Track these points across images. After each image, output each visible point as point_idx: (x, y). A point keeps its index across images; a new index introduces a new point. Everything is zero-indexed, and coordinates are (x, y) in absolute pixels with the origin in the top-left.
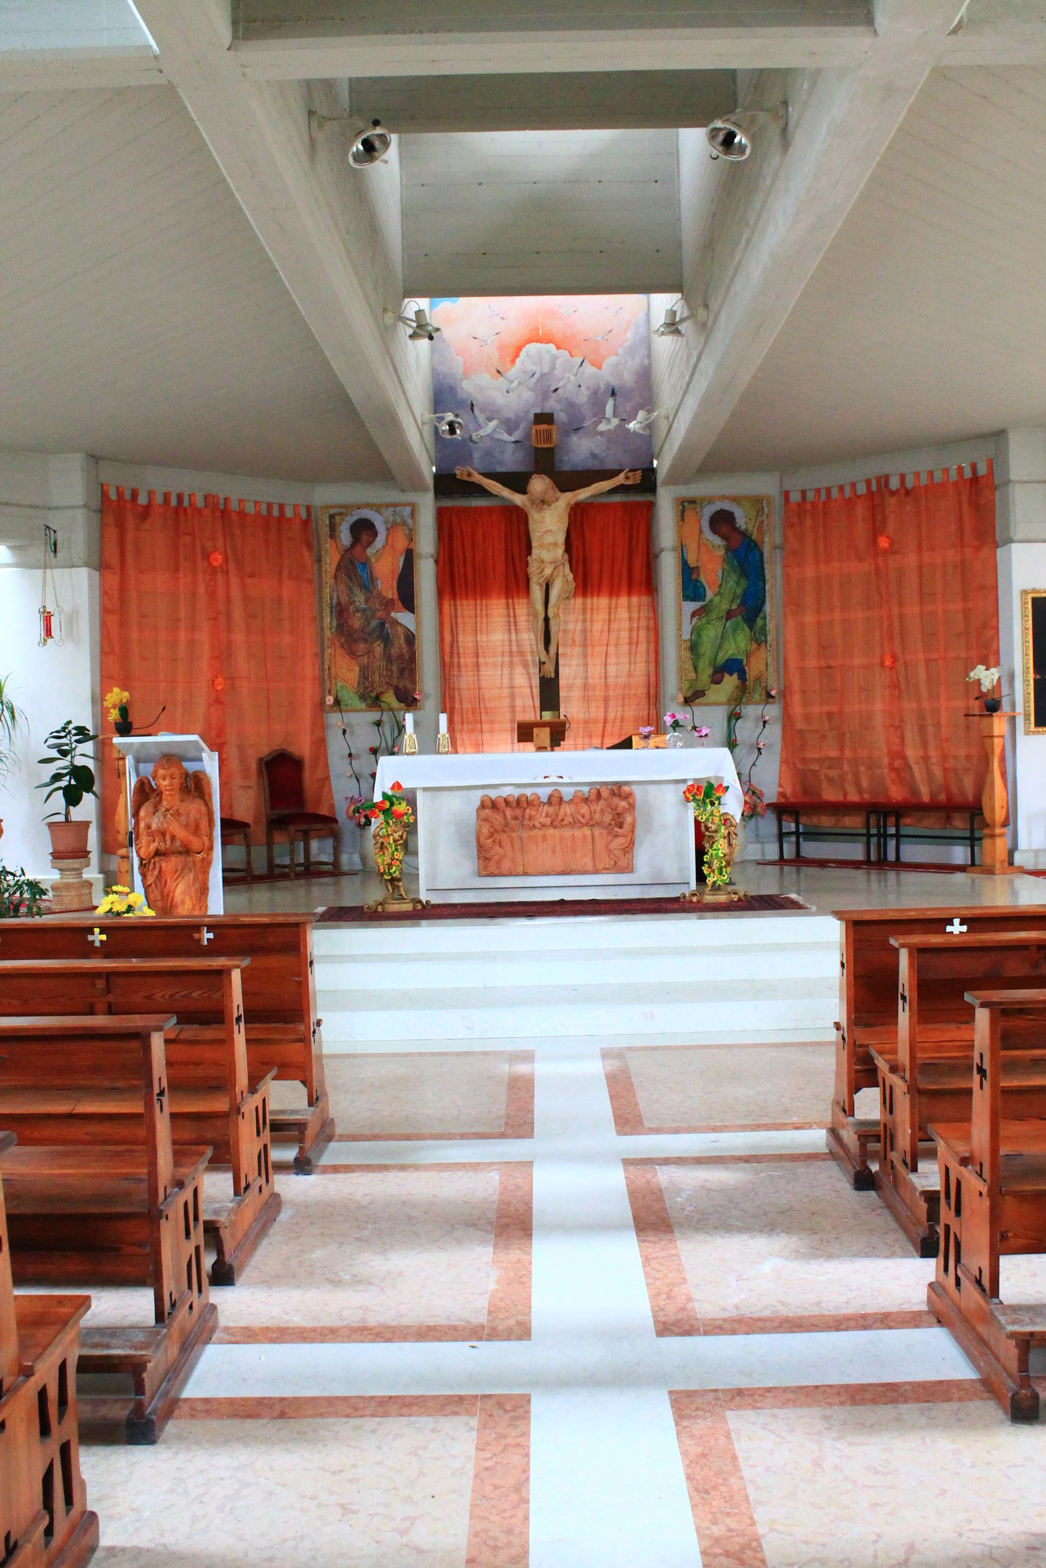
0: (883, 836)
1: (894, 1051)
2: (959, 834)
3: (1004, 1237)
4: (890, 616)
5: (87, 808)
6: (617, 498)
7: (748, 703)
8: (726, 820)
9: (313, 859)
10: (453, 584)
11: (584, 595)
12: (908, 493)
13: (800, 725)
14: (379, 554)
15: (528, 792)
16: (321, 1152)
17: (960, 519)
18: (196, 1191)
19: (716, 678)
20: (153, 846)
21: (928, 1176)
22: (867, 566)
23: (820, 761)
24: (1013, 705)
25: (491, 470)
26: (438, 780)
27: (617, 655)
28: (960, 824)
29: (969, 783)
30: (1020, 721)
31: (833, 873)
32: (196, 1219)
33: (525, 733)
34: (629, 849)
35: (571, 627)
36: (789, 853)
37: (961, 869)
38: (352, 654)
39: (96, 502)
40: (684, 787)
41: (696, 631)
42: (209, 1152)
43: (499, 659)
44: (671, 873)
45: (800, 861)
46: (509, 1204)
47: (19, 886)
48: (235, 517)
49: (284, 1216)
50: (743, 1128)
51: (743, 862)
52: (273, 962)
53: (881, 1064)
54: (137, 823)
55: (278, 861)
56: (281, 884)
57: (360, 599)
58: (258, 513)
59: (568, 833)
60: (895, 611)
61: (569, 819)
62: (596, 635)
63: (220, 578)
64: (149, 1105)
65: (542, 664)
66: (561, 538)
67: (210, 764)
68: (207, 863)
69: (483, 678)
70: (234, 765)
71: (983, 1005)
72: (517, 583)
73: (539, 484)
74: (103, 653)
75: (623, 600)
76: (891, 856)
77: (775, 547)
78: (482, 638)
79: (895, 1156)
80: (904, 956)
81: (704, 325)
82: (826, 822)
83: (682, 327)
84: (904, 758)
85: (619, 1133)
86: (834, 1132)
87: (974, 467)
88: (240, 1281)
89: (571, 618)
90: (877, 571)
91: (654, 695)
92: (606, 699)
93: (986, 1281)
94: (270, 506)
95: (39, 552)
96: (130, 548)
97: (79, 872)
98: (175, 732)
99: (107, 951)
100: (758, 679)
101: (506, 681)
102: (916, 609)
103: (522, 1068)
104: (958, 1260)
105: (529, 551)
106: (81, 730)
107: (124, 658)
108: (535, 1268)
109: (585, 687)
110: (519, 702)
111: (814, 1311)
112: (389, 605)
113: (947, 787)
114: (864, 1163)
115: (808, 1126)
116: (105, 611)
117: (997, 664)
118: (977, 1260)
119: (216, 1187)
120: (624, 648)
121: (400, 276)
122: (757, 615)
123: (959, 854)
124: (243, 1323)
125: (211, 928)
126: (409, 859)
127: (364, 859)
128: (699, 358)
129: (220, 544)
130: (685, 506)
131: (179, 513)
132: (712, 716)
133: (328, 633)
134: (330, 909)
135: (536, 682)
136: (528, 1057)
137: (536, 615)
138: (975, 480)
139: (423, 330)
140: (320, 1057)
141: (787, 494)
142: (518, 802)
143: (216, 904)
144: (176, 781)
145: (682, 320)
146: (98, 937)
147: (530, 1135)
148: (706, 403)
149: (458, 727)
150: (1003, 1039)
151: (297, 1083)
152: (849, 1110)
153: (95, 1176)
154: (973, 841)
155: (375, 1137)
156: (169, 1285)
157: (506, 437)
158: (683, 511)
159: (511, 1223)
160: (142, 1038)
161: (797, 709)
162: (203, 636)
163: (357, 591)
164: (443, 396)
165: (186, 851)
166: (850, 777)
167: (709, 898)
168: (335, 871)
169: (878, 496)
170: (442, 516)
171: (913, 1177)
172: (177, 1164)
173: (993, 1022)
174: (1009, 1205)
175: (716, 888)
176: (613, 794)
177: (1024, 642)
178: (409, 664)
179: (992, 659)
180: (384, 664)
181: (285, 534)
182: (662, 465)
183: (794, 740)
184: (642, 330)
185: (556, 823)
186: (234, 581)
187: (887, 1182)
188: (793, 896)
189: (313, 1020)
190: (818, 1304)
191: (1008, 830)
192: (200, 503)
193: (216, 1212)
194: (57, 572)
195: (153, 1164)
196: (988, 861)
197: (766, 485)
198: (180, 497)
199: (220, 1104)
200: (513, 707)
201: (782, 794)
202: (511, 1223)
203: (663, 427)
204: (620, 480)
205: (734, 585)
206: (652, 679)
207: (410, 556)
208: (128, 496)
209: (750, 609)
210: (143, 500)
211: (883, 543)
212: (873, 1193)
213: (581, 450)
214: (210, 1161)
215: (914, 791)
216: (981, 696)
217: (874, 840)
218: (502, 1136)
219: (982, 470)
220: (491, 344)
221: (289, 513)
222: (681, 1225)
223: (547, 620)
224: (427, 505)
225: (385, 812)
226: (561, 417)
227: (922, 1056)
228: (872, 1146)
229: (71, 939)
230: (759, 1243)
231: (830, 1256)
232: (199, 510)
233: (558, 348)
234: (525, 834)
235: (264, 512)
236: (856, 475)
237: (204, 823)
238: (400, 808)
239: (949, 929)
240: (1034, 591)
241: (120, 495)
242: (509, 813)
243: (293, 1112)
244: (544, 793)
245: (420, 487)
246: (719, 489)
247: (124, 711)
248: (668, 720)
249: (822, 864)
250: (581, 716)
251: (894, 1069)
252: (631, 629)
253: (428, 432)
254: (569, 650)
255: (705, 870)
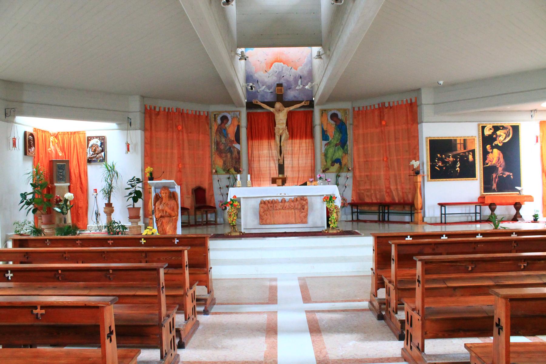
0: (384, 213)
1: (390, 277)
2: (408, 212)
3: (426, 333)
4: (386, 146)
5: (140, 203)
6: (302, 109)
7: (342, 172)
8: (336, 207)
9: (209, 219)
10: (253, 135)
11: (292, 139)
12: (391, 108)
13: (358, 179)
14: (229, 126)
15: (275, 198)
16: (212, 308)
17: (407, 116)
18: (173, 318)
19: (333, 165)
20: (160, 215)
21: (401, 315)
22: (378, 130)
23: (364, 190)
24: (424, 172)
25: (263, 101)
26: (247, 195)
27: (302, 157)
28: (407, 209)
29: (410, 196)
30: (426, 178)
31: (368, 224)
32: (173, 327)
33: (274, 181)
34: (306, 216)
35: (288, 149)
36: (355, 218)
37: (408, 223)
38: (221, 157)
39: (143, 111)
40: (323, 197)
41: (326, 150)
42: (177, 307)
43: (266, 158)
44: (319, 224)
45: (358, 221)
46: (270, 324)
47: (119, 227)
48: (185, 115)
49: (200, 327)
50: (342, 301)
51: (341, 221)
52: (197, 249)
53: (386, 281)
54: (155, 207)
55: (198, 220)
56: (198, 227)
57: (223, 140)
58: (192, 114)
59: (287, 211)
60: (387, 144)
61: (287, 207)
62: (296, 151)
63: (181, 133)
64: (159, 291)
65: (279, 160)
66: (285, 122)
67: (177, 189)
68: (176, 220)
69: (261, 164)
70: (185, 190)
71: (419, 260)
72: (271, 135)
73: (278, 105)
74: (145, 156)
75: (304, 141)
76: (386, 219)
77: (350, 124)
78: (261, 152)
79: (390, 309)
80: (393, 247)
81: (329, 55)
82: (366, 208)
83: (322, 57)
84: (390, 189)
85: (304, 303)
86: (371, 302)
87: (411, 100)
88: (187, 347)
89: (288, 146)
90: (382, 131)
91: (313, 170)
92: (299, 171)
93: (420, 347)
94: (196, 112)
95: (126, 125)
96: (153, 124)
97: (137, 223)
98: (166, 179)
99: (145, 245)
100: (345, 165)
101: (268, 166)
102: (394, 143)
103: (273, 283)
104: (411, 341)
105: (275, 126)
106: (138, 179)
107: (151, 158)
108: (279, 344)
109: (292, 167)
110: (272, 172)
111: (365, 357)
112: (232, 142)
113: (403, 197)
114: (380, 312)
115: (363, 301)
116: (146, 143)
117: (419, 160)
118: (417, 340)
119: (179, 319)
120: (304, 155)
121: (236, 40)
122: (345, 145)
123: (407, 218)
124: (188, 360)
125: (178, 238)
126: (238, 220)
127: (224, 220)
128: (327, 66)
129: (181, 123)
130: (323, 112)
131: (168, 114)
132: (331, 176)
133: (213, 151)
134: (214, 235)
135: (277, 165)
136: (275, 280)
137: (277, 145)
138: (411, 104)
139: (243, 57)
140: (211, 279)
141: (354, 108)
142: (272, 202)
143: (179, 231)
144: (167, 195)
145: (322, 54)
146: (143, 241)
147: (276, 303)
148: (330, 79)
149: (253, 179)
150: (426, 271)
151: (204, 287)
152: (376, 295)
153: (142, 313)
154: (411, 214)
155: (228, 304)
156: (165, 348)
157: (268, 91)
158: (322, 113)
159: (271, 330)
160: (157, 270)
161: (357, 174)
162: (175, 151)
163: (222, 137)
164: (249, 78)
165: (170, 216)
166: (373, 195)
167: (331, 231)
168: (215, 223)
169: (382, 109)
170: (248, 115)
171: (396, 316)
172: (167, 310)
173: (422, 265)
174: (427, 323)
175: (333, 228)
176: (301, 199)
177: (427, 153)
178: (238, 160)
179: (417, 158)
180: (230, 160)
181: (200, 120)
182: (316, 99)
183: (356, 183)
184: (310, 59)
185: (284, 208)
186: (185, 135)
187: (388, 318)
188: (357, 231)
189: (209, 267)
190: (367, 355)
191: (422, 211)
192: (175, 111)
193: (179, 325)
194: (131, 132)
195: (160, 309)
196: (416, 220)
197: (347, 105)
198: (169, 109)
199: (181, 292)
200: (270, 173)
201: (353, 200)
202: (271, 330)
203: (316, 87)
204: (303, 104)
205: (338, 136)
206: (313, 165)
207: (239, 127)
208: (153, 108)
209: (343, 143)
210: (157, 110)
211: (383, 123)
212: (383, 321)
213: (291, 95)
214: (178, 310)
215: (394, 199)
216: (414, 170)
217: (381, 214)
218: (267, 303)
219: (413, 101)
220: (263, 63)
221: (202, 114)
222: (324, 331)
223: (280, 147)
224: (244, 112)
225: (231, 204)
226: (285, 85)
227: (399, 278)
228: (383, 306)
229: (135, 241)
230: (348, 336)
231: (370, 340)
232: (174, 113)
233: (284, 64)
234: (274, 212)
235: (194, 113)
236: (375, 102)
237: (175, 208)
238: (235, 204)
239: (406, 239)
240: (430, 137)
241: (151, 109)
242: (269, 205)
243: (203, 295)
244: (280, 199)
245: (242, 106)
246: (333, 107)
247: (151, 174)
248: (318, 177)
249: (365, 221)
250: (291, 176)
251: (390, 282)
252: (306, 150)
253: (244, 89)
254: (287, 156)
255: (330, 223)
